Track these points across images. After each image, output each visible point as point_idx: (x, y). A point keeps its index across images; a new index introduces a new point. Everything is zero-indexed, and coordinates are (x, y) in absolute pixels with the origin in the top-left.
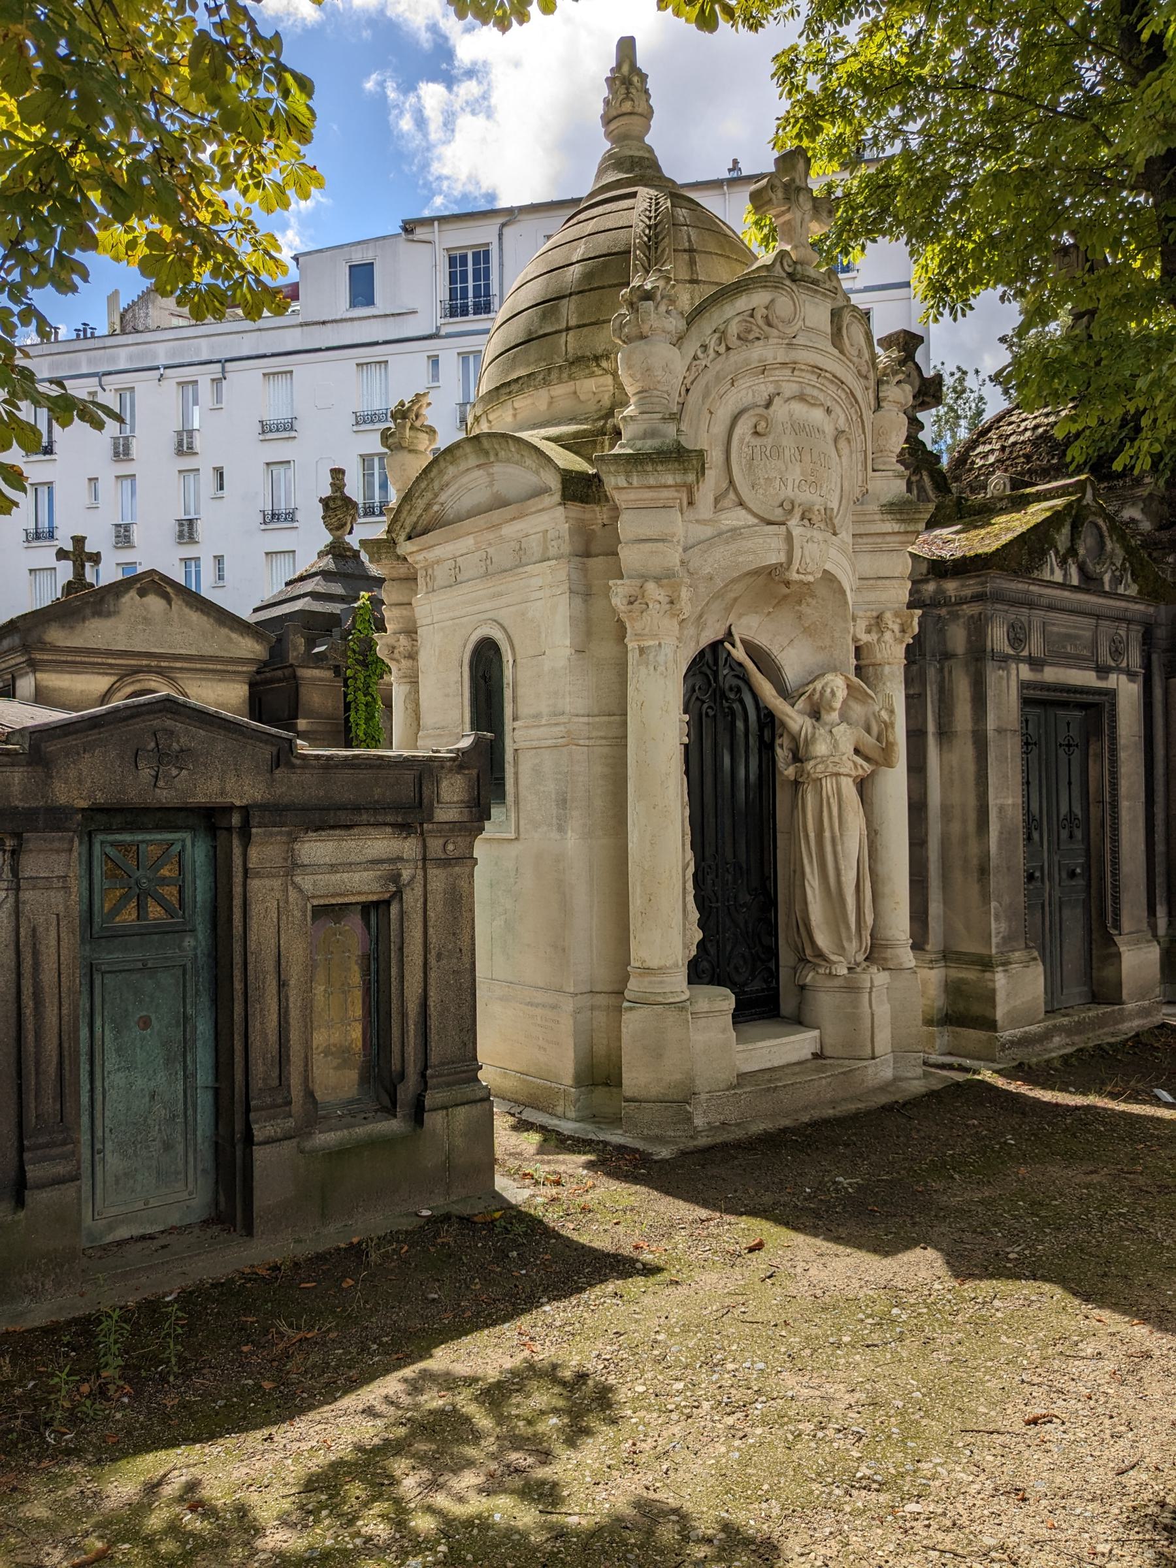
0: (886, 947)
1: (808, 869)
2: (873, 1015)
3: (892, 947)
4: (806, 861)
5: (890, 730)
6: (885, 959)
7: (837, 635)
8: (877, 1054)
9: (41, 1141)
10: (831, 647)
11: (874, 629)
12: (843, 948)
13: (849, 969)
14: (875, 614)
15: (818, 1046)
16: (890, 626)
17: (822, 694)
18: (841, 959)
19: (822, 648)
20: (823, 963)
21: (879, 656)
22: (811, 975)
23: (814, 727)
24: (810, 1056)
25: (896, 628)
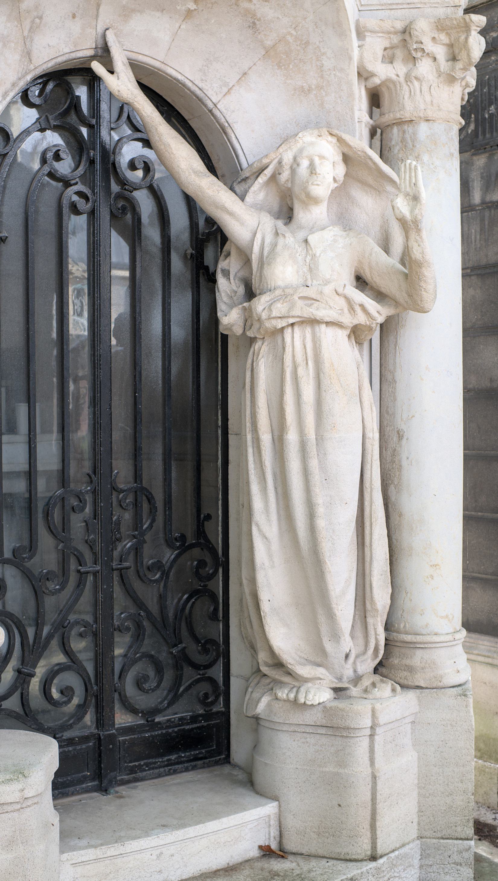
0: (413, 646)
1: (257, 504)
2: (374, 777)
3: (424, 646)
4: (255, 488)
5: (413, 235)
6: (411, 669)
7: (328, 64)
8: (380, 851)
9: (166, 702)
10: (319, 87)
11: (399, 53)
12: (323, 652)
13: (337, 690)
14: (399, 26)
15: (274, 832)
16: (430, 47)
17: (293, 171)
18: (321, 672)
19: (304, 91)
20: (286, 679)
21: (409, 106)
22: (265, 700)
23: (277, 234)
24: (255, 853)
25: (440, 52)
